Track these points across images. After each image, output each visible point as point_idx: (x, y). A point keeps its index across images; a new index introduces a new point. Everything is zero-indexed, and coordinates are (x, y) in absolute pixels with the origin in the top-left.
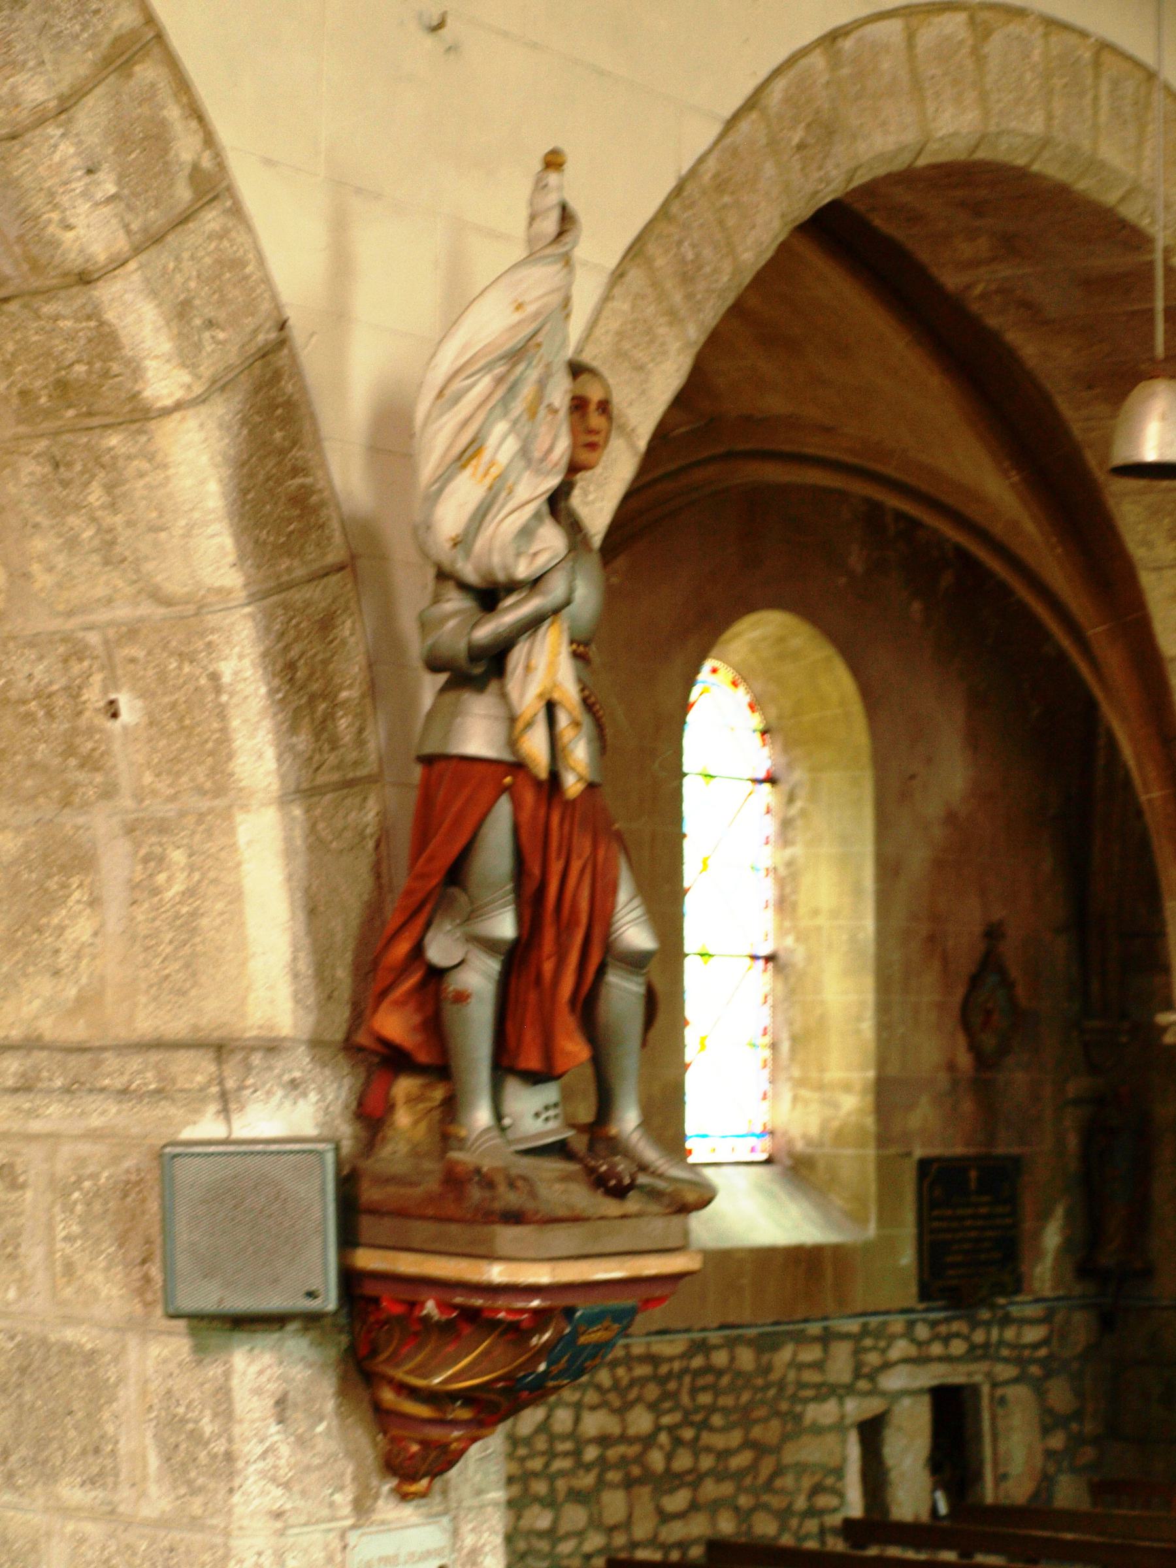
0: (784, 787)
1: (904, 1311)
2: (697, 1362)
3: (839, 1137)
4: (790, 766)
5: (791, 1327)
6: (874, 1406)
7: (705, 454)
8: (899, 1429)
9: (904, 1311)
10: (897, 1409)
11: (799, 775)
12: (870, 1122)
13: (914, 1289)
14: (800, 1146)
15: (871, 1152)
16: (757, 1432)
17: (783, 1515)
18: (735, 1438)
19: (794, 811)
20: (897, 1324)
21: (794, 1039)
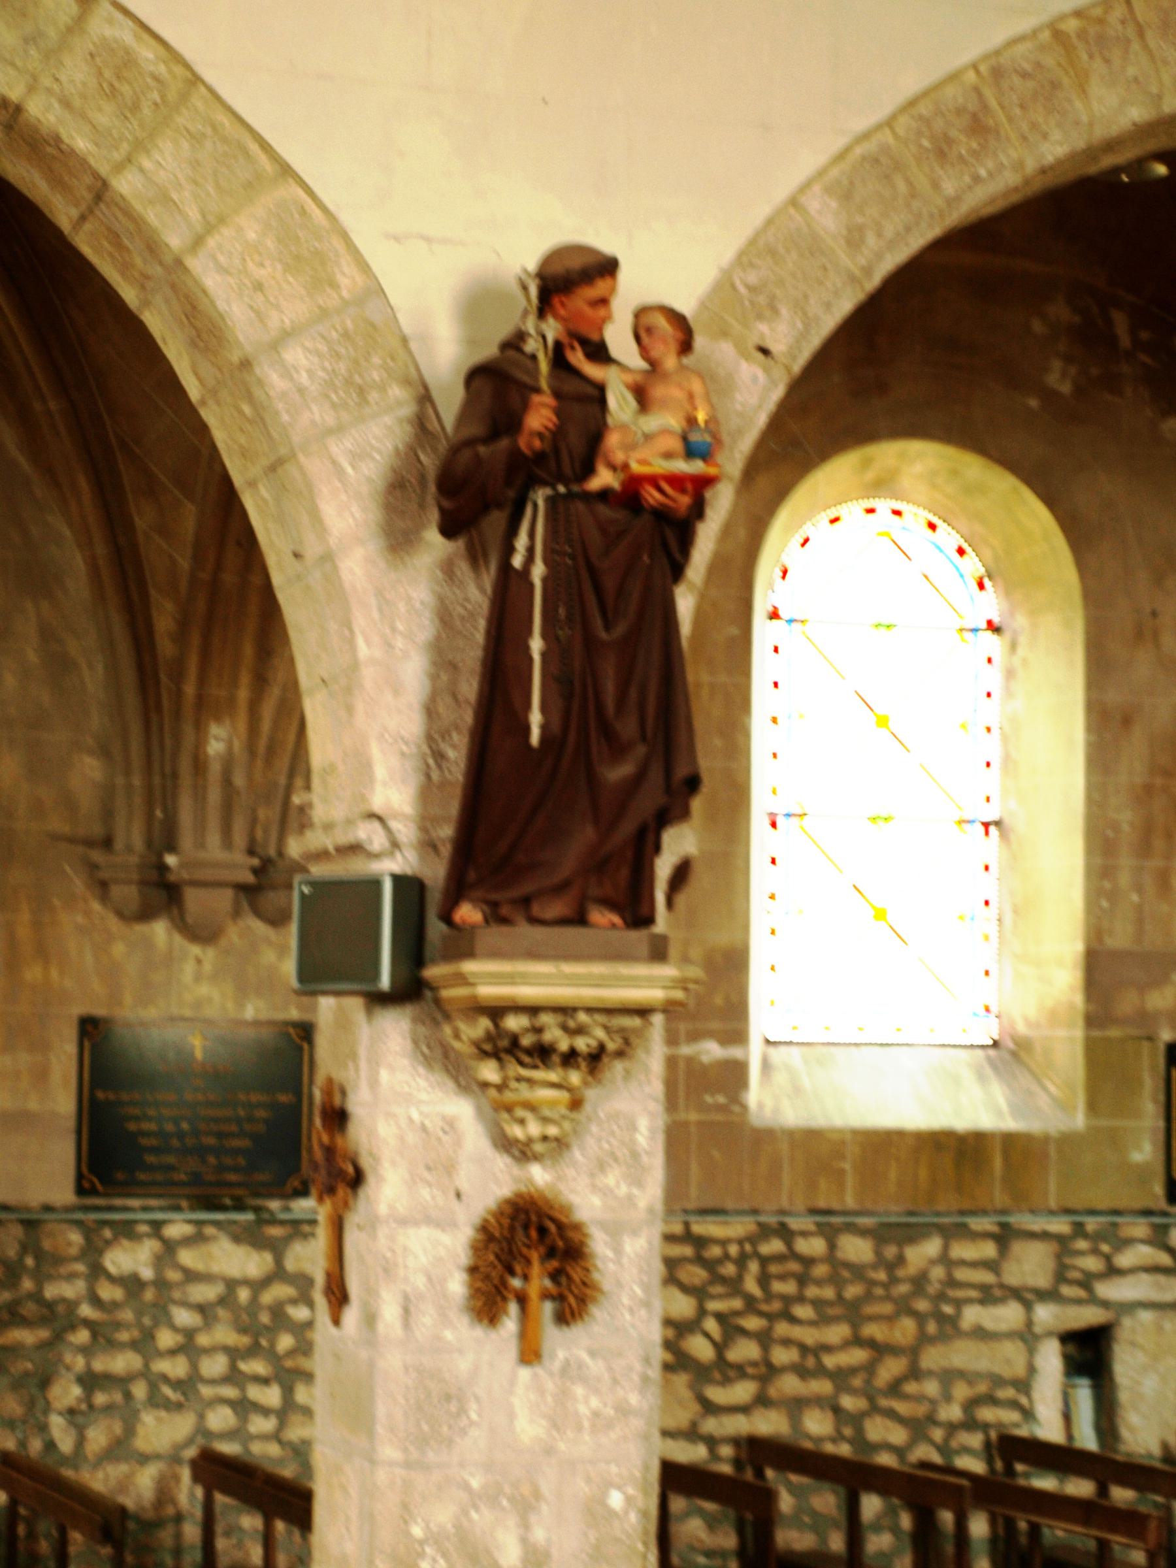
0: (1007, 635)
1: (1147, 1213)
2: (775, 1246)
3: (1053, 1017)
4: (1012, 613)
5: (936, 1220)
6: (1087, 1316)
7: (314, 206)
8: (1133, 1344)
9: (1147, 1213)
10: (1127, 1322)
11: (1021, 621)
12: (1079, 999)
13: (1159, 1188)
14: (1021, 1029)
15: (1079, 1033)
16: (872, 1330)
17: (918, 1428)
18: (837, 1333)
19: (1016, 661)
20: (1139, 1228)
21: (1016, 911)
